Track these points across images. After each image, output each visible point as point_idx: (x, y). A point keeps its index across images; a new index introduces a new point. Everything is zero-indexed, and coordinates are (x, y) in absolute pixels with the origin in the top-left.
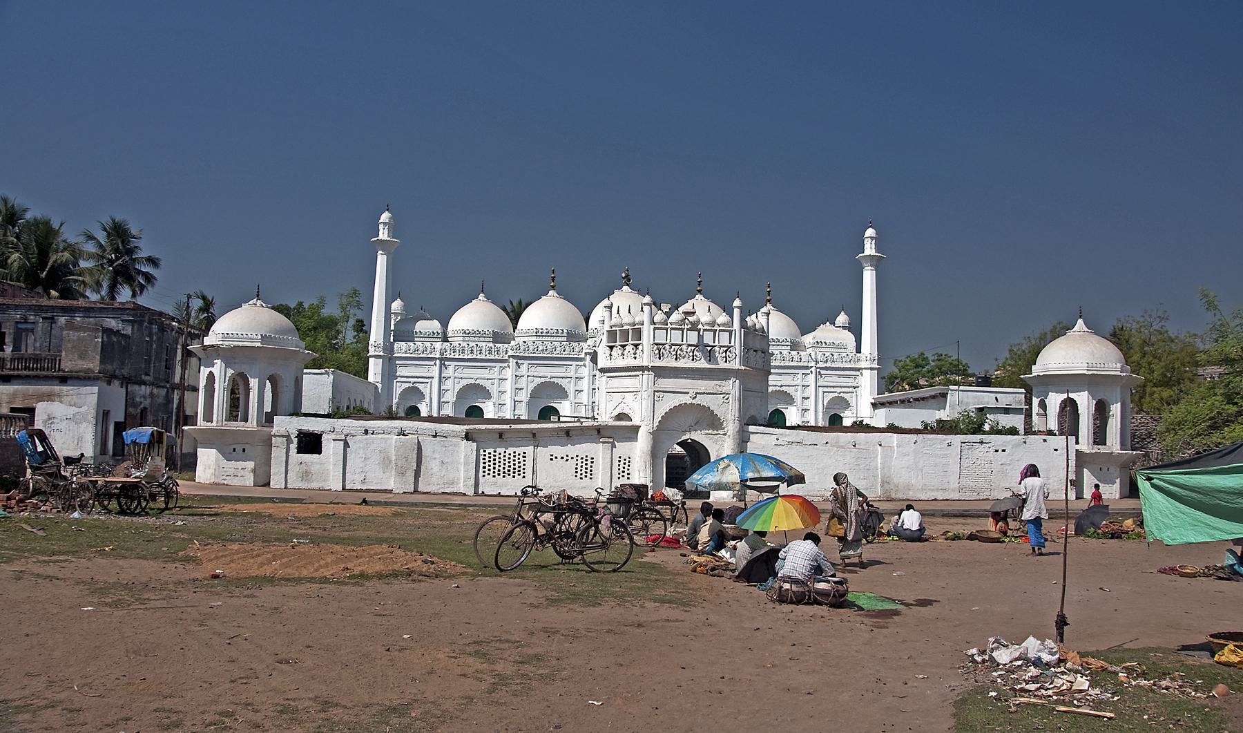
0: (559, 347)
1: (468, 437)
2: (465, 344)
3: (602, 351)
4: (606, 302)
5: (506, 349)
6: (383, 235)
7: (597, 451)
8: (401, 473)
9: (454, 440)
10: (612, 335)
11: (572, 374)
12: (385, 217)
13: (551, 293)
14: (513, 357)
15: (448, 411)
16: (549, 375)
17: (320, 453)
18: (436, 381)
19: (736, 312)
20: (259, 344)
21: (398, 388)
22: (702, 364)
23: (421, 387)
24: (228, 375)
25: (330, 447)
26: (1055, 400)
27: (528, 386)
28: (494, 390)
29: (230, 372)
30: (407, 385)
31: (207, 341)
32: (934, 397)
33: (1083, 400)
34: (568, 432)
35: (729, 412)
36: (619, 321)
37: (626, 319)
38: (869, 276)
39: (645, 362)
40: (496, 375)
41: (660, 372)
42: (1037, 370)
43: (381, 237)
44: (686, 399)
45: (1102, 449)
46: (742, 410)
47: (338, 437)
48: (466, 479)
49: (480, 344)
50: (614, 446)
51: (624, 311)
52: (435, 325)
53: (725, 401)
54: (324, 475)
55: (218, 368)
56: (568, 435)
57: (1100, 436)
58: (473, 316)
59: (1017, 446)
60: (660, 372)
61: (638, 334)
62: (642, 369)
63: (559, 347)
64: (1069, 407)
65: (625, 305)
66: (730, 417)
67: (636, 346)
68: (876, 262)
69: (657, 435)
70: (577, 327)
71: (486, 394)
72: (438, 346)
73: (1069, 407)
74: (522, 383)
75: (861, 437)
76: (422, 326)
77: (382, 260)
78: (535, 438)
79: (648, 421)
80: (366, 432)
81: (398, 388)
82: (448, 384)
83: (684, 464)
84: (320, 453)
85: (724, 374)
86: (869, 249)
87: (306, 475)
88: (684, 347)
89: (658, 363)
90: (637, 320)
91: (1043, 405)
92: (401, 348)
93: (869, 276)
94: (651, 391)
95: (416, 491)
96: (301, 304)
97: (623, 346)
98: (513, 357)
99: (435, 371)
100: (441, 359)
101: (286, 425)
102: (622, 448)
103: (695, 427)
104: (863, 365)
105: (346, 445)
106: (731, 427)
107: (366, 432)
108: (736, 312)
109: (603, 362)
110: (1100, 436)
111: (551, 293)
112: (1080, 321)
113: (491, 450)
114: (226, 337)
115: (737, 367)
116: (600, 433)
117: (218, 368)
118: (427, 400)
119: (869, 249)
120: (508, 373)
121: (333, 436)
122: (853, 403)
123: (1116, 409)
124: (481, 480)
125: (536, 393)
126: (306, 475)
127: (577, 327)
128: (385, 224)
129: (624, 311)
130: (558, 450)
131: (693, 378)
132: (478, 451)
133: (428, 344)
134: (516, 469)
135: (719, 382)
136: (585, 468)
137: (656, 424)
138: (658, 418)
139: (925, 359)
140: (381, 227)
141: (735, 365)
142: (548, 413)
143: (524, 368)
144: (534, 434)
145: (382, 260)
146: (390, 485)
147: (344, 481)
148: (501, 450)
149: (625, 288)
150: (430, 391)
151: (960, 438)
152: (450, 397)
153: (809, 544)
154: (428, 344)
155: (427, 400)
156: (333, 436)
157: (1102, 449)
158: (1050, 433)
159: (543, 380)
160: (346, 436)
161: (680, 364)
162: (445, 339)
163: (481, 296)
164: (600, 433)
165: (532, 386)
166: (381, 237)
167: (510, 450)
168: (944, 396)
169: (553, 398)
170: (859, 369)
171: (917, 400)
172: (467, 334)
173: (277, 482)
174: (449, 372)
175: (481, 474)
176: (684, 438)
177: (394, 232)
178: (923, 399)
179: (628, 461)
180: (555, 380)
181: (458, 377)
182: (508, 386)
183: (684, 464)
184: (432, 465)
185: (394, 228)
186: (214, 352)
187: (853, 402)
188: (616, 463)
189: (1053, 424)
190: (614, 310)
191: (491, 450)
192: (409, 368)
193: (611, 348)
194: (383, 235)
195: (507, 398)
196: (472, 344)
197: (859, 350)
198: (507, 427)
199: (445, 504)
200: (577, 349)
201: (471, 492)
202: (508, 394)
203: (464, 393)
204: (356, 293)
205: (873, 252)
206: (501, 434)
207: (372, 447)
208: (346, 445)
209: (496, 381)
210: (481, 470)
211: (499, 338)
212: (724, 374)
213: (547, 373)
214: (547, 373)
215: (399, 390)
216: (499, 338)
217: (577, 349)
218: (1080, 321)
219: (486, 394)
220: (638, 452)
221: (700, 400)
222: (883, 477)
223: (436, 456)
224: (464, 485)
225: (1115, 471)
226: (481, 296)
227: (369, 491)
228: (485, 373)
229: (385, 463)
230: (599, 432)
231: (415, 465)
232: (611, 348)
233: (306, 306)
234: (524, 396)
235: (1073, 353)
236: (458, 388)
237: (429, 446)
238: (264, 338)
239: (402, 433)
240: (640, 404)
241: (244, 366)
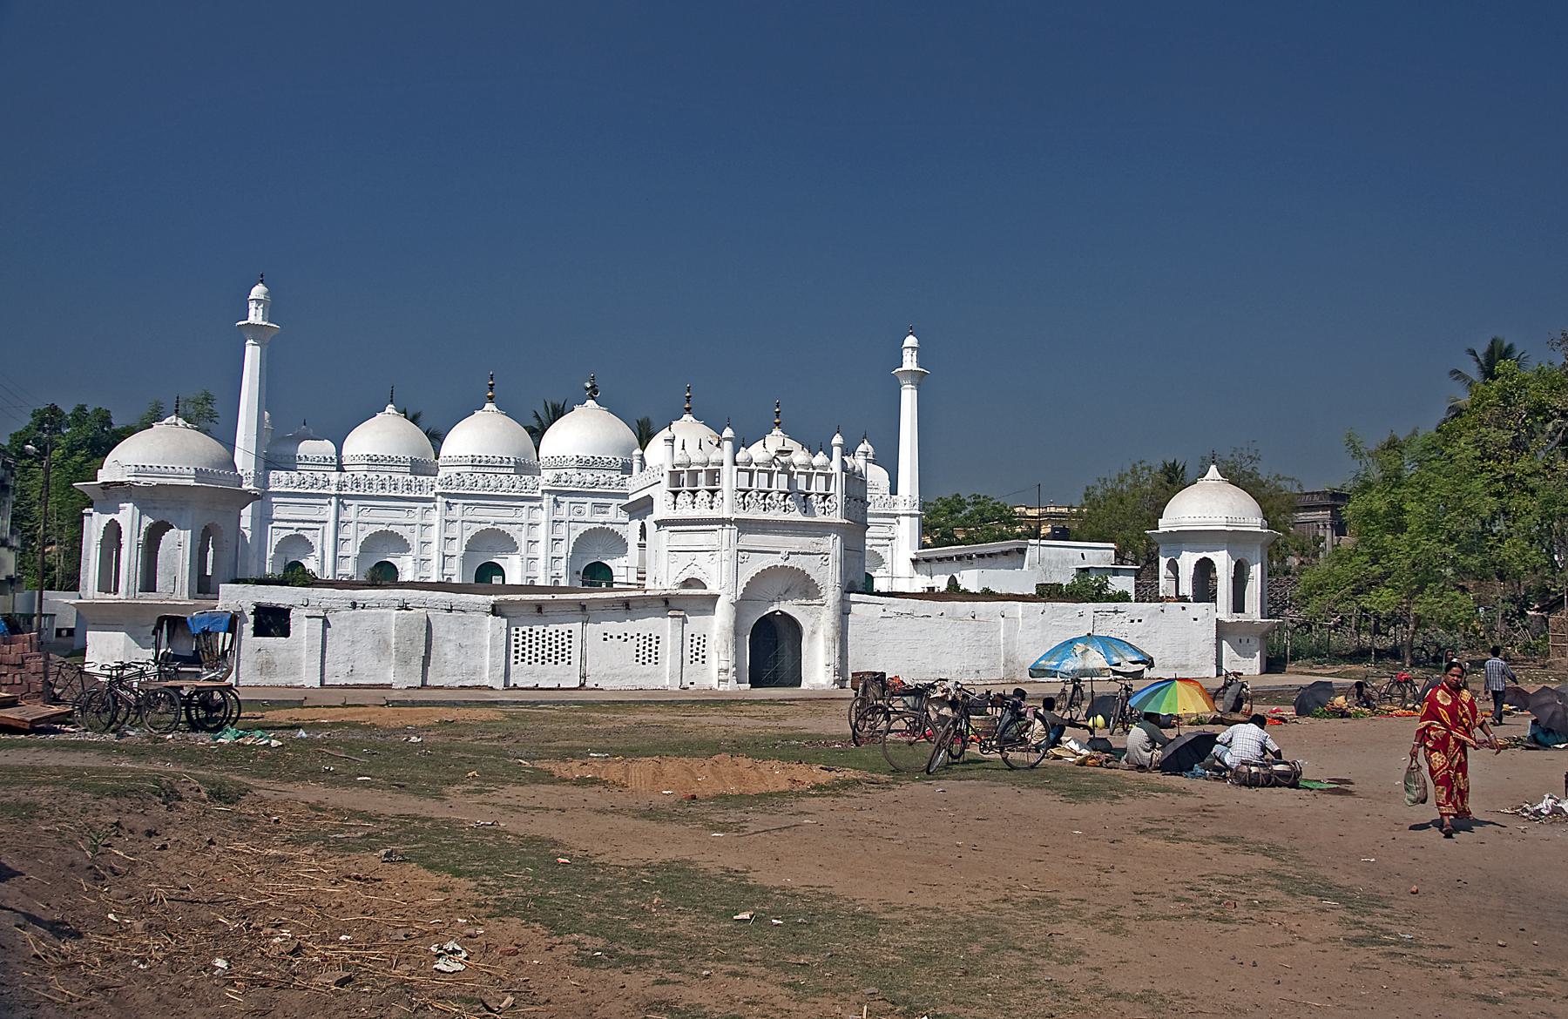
0: (506, 483)
1: (495, 610)
2: (372, 476)
3: (661, 495)
4: (665, 433)
5: (431, 485)
6: (255, 316)
7: (664, 627)
8: (404, 661)
9: (476, 615)
10: (675, 476)
11: (524, 519)
12: (258, 291)
13: (488, 406)
14: (442, 494)
15: (348, 569)
16: (492, 520)
17: (287, 634)
18: (330, 527)
19: (837, 452)
20: (192, 482)
21: (275, 537)
22: (797, 516)
23: (308, 535)
24: (145, 525)
25: (302, 626)
26: (1188, 561)
27: (462, 535)
28: (414, 539)
29: (148, 521)
30: (289, 532)
31: (104, 476)
32: (1006, 553)
33: (1223, 562)
34: (627, 604)
35: (829, 576)
36: (686, 460)
37: (697, 457)
38: (909, 397)
39: (726, 516)
40: (417, 519)
41: (745, 526)
42: (1165, 525)
43: (252, 319)
44: (776, 560)
45: (1242, 617)
46: (844, 573)
47: (314, 613)
48: (493, 667)
49: (395, 476)
50: (685, 621)
51: (692, 448)
52: (327, 447)
53: (824, 563)
54: (293, 666)
55: (127, 515)
56: (628, 608)
57: (1238, 606)
58: (379, 436)
59: (1156, 614)
60: (745, 526)
61: (713, 476)
62: (722, 522)
63: (506, 483)
64: (1205, 569)
65: (687, 438)
66: (830, 583)
67: (713, 492)
68: (919, 379)
69: (739, 606)
70: (527, 455)
71: (403, 546)
72: (334, 477)
73: (1205, 569)
74: (455, 530)
75: (982, 606)
76: (307, 448)
77: (252, 354)
78: (584, 611)
79: (730, 588)
80: (354, 605)
81: (275, 537)
82: (348, 532)
83: (770, 647)
84: (287, 634)
85: (823, 529)
86: (910, 362)
87: (266, 667)
88: (774, 495)
89: (743, 515)
90: (713, 458)
91: (1173, 567)
92: (279, 480)
93: (909, 397)
94: (733, 550)
95: (424, 685)
96: (82, 408)
97: (694, 493)
98: (442, 494)
99: (330, 512)
100: (338, 496)
101: (236, 598)
102: (695, 623)
103: (786, 594)
104: (900, 509)
105: (326, 624)
106: (831, 595)
107: (354, 605)
108: (837, 452)
109: (662, 510)
110: (1238, 606)
111: (488, 406)
112: (1213, 467)
113: (526, 629)
114: (140, 470)
115: (839, 520)
116: (666, 604)
117: (127, 515)
118: (318, 553)
119: (910, 362)
120: (435, 517)
121: (307, 612)
122: (887, 559)
123: (1256, 571)
124: (513, 668)
125: (473, 545)
126: (266, 667)
127: (527, 455)
128: (258, 301)
129: (692, 448)
130: (612, 627)
131: (784, 534)
132: (508, 629)
133: (320, 475)
134: (558, 654)
135: (816, 539)
136: (649, 651)
137: (740, 592)
138: (742, 585)
139: (960, 502)
140: (252, 305)
141: (836, 517)
142: (597, 574)
143: (457, 510)
144: (583, 607)
145: (252, 354)
146: (389, 678)
147: (322, 674)
148: (540, 628)
149: (590, 402)
150: (322, 541)
151: (1092, 606)
152: (351, 549)
153: (1253, 728)
154: (320, 475)
155: (318, 553)
156: (307, 612)
157: (1242, 617)
158: (1184, 599)
159: (484, 527)
160: (326, 611)
161: (770, 516)
162: (340, 469)
163: (390, 408)
164: (666, 604)
165: (468, 535)
166: (252, 319)
167: (551, 628)
168: (1022, 551)
169: (494, 551)
170: (895, 516)
171: (981, 556)
172: (373, 461)
173: (649, 584)
174: (350, 514)
175: (513, 660)
176: (771, 610)
177: (270, 315)
178: (990, 555)
179: (702, 640)
180: (501, 527)
181: (362, 523)
182: (434, 534)
183: (770, 647)
184: (445, 649)
185: (272, 308)
186: (117, 492)
187: (887, 557)
188: (687, 643)
189: (1186, 588)
190: (678, 444)
191: (526, 629)
192: (291, 508)
193: (676, 494)
194: (255, 316)
195: (536, 559)
196: (382, 476)
197: (894, 490)
198: (549, 597)
199: (477, 698)
200: (531, 485)
201: (500, 685)
202: (435, 546)
203: (369, 545)
204: (208, 399)
205: (915, 368)
206: (539, 608)
207: (363, 625)
208: (326, 624)
209: (417, 528)
210: (513, 655)
211: (419, 468)
212: (823, 529)
213: (489, 517)
214: (489, 517)
215: (275, 543)
216: (419, 468)
217: (531, 485)
218: (1213, 467)
219: (403, 546)
220: (718, 626)
221: (794, 562)
222: (1007, 654)
223: (452, 637)
224: (490, 676)
225: (1255, 643)
226: (390, 408)
227: (358, 686)
228: (402, 517)
229: (382, 647)
230: (667, 602)
231: (423, 649)
232: (676, 494)
233: (89, 410)
234: (457, 549)
235: (1206, 505)
236: (362, 537)
237: (441, 623)
238: (199, 474)
239: (404, 607)
240: (721, 568)
241: (168, 513)
